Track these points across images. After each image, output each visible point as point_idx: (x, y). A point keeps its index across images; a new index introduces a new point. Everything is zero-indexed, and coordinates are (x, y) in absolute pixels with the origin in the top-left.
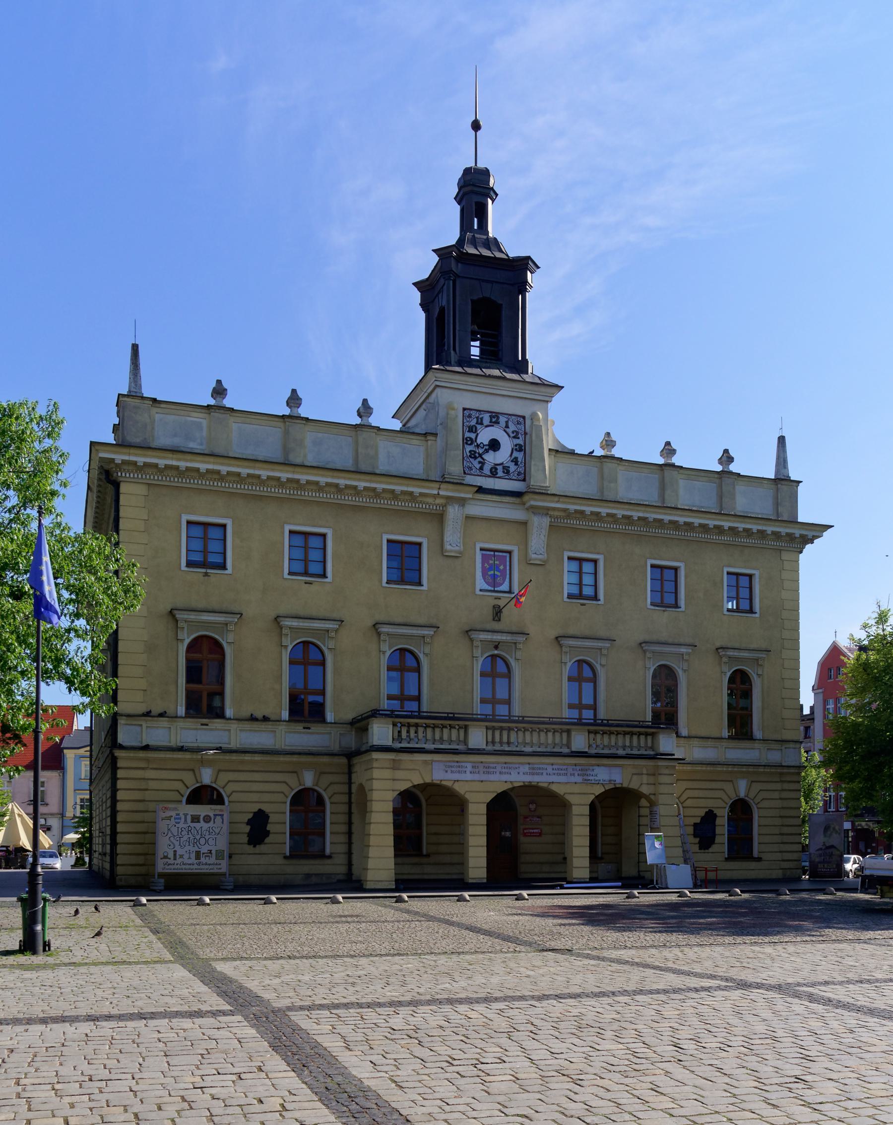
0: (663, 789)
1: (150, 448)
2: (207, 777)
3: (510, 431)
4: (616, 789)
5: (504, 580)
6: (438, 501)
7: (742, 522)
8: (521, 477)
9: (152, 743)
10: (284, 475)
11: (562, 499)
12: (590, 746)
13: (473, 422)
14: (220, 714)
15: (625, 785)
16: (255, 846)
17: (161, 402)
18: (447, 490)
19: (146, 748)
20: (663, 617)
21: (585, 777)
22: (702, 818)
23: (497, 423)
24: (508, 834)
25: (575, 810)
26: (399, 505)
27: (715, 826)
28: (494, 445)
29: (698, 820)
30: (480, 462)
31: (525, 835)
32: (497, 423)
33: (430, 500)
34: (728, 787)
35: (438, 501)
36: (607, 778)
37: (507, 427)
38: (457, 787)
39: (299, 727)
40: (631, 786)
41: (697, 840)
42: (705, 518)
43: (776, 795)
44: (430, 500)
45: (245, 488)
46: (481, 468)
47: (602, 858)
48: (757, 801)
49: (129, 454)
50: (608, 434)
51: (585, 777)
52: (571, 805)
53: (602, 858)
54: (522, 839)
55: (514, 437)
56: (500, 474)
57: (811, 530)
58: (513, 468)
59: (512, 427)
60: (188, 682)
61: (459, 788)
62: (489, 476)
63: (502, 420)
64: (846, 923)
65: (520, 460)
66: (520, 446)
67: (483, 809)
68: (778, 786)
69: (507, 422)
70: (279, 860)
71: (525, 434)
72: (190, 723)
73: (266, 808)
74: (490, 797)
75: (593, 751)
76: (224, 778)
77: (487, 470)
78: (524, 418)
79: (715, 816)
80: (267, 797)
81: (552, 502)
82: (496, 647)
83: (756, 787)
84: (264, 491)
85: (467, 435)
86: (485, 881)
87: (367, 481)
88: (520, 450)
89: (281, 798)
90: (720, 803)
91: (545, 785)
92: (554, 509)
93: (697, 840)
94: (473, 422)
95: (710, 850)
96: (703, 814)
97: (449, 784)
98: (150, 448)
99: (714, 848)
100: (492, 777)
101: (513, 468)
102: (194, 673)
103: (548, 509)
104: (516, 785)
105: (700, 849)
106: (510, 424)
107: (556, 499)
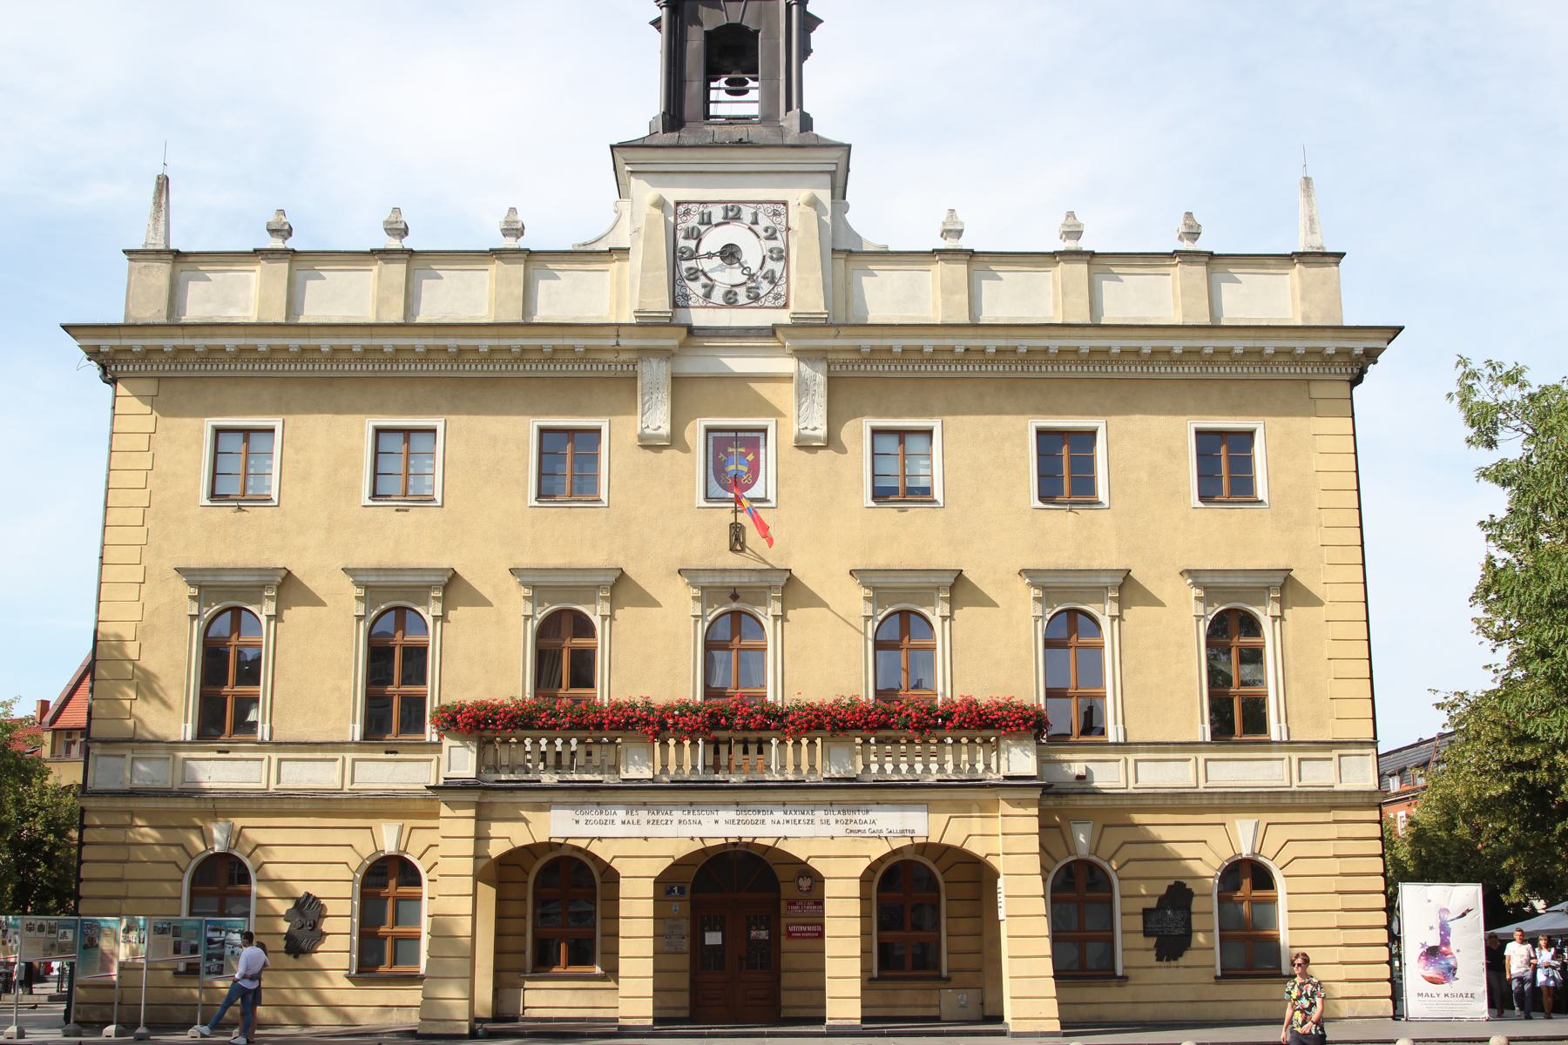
3: (759, 229)
4: (372, 865)
5: (755, 479)
6: (623, 357)
7: (1208, 338)
8: (781, 302)
10: (294, 343)
11: (843, 331)
13: (693, 221)
15: (934, 839)
16: (296, 957)
17: (186, 254)
18: (631, 337)
20: (1227, 519)
21: (852, 826)
22: (1162, 899)
24: (763, 934)
26: (558, 369)
27: (1190, 913)
28: (730, 254)
29: (1153, 903)
30: (705, 286)
31: (789, 934)
32: (737, 218)
33: (610, 357)
35: (623, 357)
36: (897, 827)
37: (755, 222)
38: (596, 849)
40: (946, 841)
41: (1152, 941)
42: (1131, 338)
44: (610, 357)
45: (303, 369)
46: (707, 296)
47: (948, 979)
49: (120, 337)
50: (1189, 215)
51: (852, 826)
52: (995, 875)
53: (948, 979)
54: (785, 943)
55: (767, 238)
56: (742, 298)
57: (898, 337)
59: (764, 221)
61: (601, 851)
62: (721, 307)
65: (778, 275)
66: (781, 251)
67: (648, 888)
69: (756, 214)
71: (788, 229)
73: (316, 890)
77: (718, 296)
78: (785, 203)
79: (1189, 895)
81: (828, 337)
82: (735, 597)
84: (1114, 371)
86: (650, 1022)
87: (493, 337)
88: (779, 259)
89: (172, 872)
91: (769, 842)
92: (835, 350)
93: (1152, 941)
94: (693, 221)
95: (1182, 961)
96: (1163, 891)
97: (582, 844)
99: (1188, 958)
100: (662, 830)
103: (826, 351)
104: (710, 843)
105: (1159, 958)
106: (760, 216)
107: (833, 331)
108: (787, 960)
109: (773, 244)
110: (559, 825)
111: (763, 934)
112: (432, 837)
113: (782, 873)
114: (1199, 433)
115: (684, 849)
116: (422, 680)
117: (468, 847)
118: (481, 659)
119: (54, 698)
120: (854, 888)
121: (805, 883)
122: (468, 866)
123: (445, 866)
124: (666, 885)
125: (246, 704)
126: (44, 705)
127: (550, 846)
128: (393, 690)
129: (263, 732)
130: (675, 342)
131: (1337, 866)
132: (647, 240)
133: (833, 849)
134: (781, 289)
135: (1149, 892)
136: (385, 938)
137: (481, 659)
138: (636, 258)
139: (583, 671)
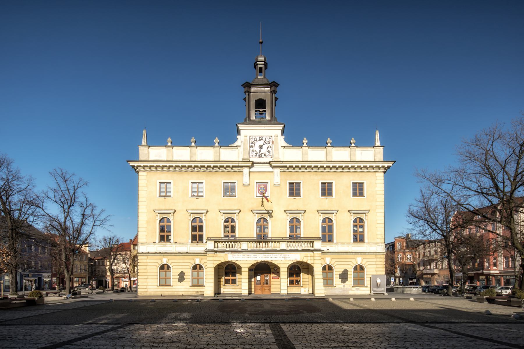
0: (316, 262)
1: (280, 161)
2: (197, 261)
9: (150, 251)
12: (215, 247)
14: (169, 241)
19: (149, 253)
23: (262, 139)
24: (268, 278)
25: (281, 270)
28: (261, 147)
32: (262, 139)
34: (353, 261)
38: (237, 262)
39: (195, 245)
43: (374, 263)
48: (334, 265)
54: (272, 280)
58: (267, 154)
60: (322, 232)
63: (264, 138)
64: (474, 313)
67: (247, 270)
68: (375, 260)
70: (156, 287)
72: (160, 245)
73: (184, 271)
74: (249, 266)
75: (249, 249)
76: (170, 261)
79: (348, 271)
80: (184, 267)
83: (365, 260)
85: (251, 145)
90: (350, 266)
98: (280, 161)
101: (267, 154)
102: (162, 230)
108: (272, 283)
109: (269, 145)
110: (231, 257)
111: (268, 278)
112: (205, 261)
113: (271, 267)
114: (353, 183)
115: (253, 263)
116: (202, 232)
117: (212, 262)
118: (214, 228)
119: (133, 239)
120: (286, 270)
121: (276, 269)
122: (139, 284)
123: (208, 266)
124: (250, 270)
125: (168, 236)
126: (131, 240)
127: (228, 262)
128: (197, 234)
129: (172, 241)
130: (250, 165)
131: (375, 266)
132: (244, 144)
133: (282, 262)
134: (271, 154)
135: (341, 271)
136: (97, 287)
137: (214, 228)
138: (242, 148)
139: (233, 229)
